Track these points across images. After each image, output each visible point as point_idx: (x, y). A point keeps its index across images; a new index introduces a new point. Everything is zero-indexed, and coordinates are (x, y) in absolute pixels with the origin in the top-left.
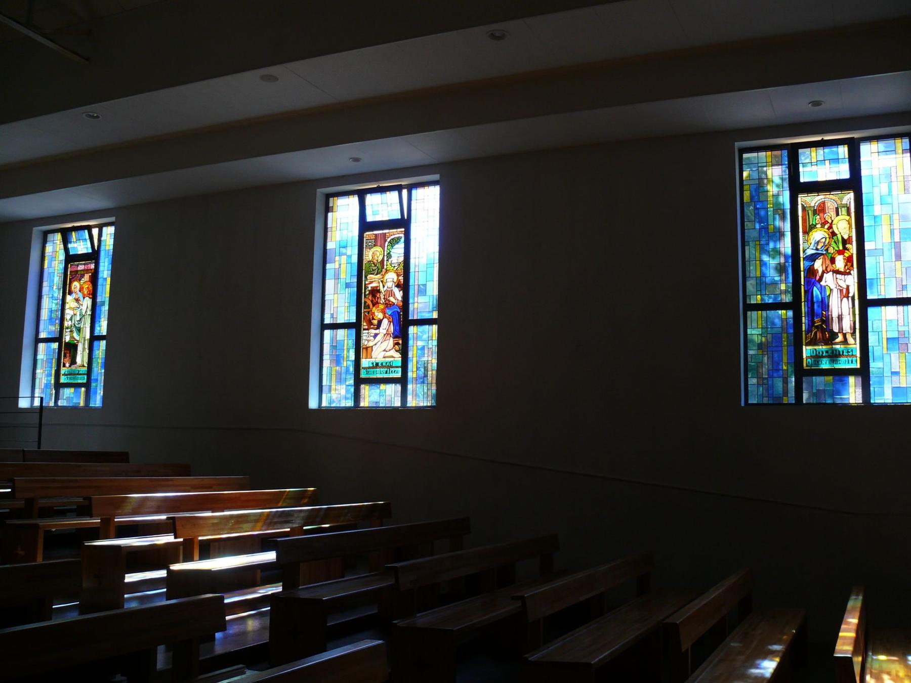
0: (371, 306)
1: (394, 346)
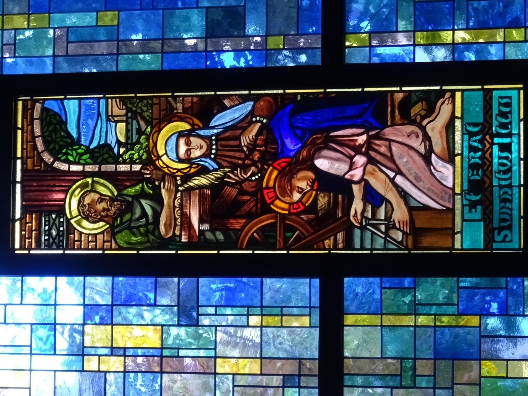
0: (266, 220)
1: (412, 122)
